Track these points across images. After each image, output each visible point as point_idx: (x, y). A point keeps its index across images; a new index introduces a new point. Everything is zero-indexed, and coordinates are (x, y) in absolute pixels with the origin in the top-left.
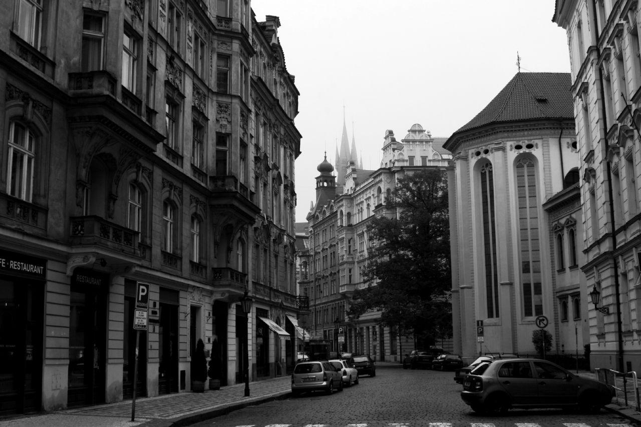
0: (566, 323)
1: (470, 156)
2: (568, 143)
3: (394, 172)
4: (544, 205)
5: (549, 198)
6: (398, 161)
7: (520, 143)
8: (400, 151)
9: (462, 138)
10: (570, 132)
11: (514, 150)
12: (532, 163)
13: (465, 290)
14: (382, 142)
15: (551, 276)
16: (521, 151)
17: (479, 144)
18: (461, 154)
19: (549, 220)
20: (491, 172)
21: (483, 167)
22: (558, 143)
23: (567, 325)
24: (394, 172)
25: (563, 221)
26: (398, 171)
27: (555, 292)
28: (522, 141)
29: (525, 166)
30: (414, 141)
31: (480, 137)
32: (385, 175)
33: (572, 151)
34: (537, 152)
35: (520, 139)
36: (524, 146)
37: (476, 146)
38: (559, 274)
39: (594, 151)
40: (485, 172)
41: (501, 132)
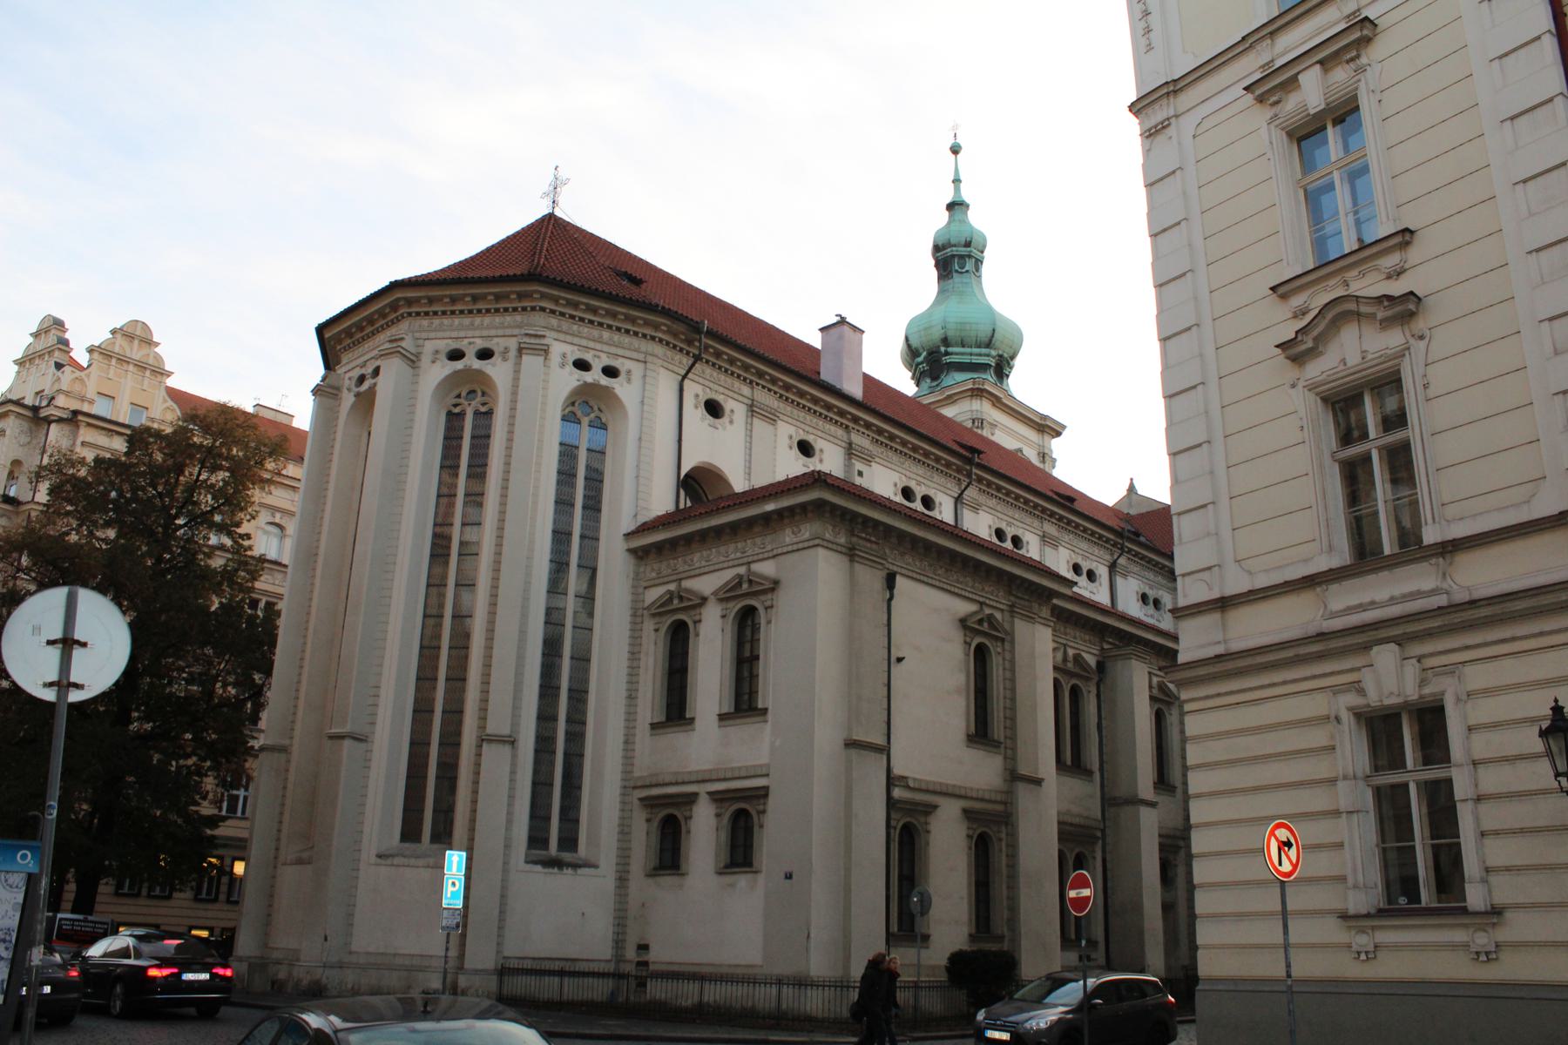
0: (668, 880)
1: (425, 360)
3: (48, 421)
4: (628, 536)
6: (67, 394)
7: (588, 357)
9: (410, 302)
11: (570, 367)
13: (347, 743)
14: (21, 342)
16: (588, 377)
18: (403, 344)
22: (676, 387)
24: (48, 421)
25: (707, 584)
26: (60, 420)
29: (585, 421)
30: (123, 360)
31: (470, 312)
32: (18, 422)
33: (703, 419)
35: (591, 344)
36: (597, 367)
39: (1412, 232)
41: (543, 309)
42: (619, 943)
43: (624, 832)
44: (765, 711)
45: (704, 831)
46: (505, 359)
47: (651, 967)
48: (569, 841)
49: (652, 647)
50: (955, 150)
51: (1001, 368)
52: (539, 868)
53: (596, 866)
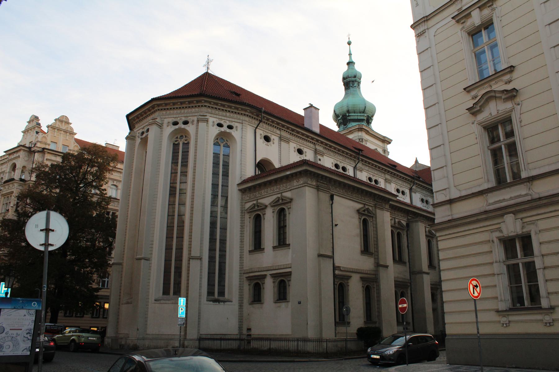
0: (257, 306)
1: (165, 125)
3: (34, 152)
4: (238, 185)
5: (243, 179)
6: (41, 142)
7: (222, 122)
8: (44, 135)
9: (159, 105)
11: (216, 126)
13: (143, 261)
14: (24, 125)
15: (239, 257)
16: (222, 129)
17: (179, 114)
19: (242, 199)
23: (262, 308)
24: (34, 152)
27: (242, 272)
29: (222, 145)
30: (59, 130)
32: (24, 153)
35: (223, 118)
36: (225, 126)
37: (175, 116)
39: (514, 67)
40: (179, 144)
41: (205, 106)
42: (240, 328)
44: (289, 245)
45: (269, 288)
46: (193, 124)
47: (252, 336)
48: (222, 293)
49: (248, 223)
50: (349, 43)
51: (369, 120)
52: (211, 303)
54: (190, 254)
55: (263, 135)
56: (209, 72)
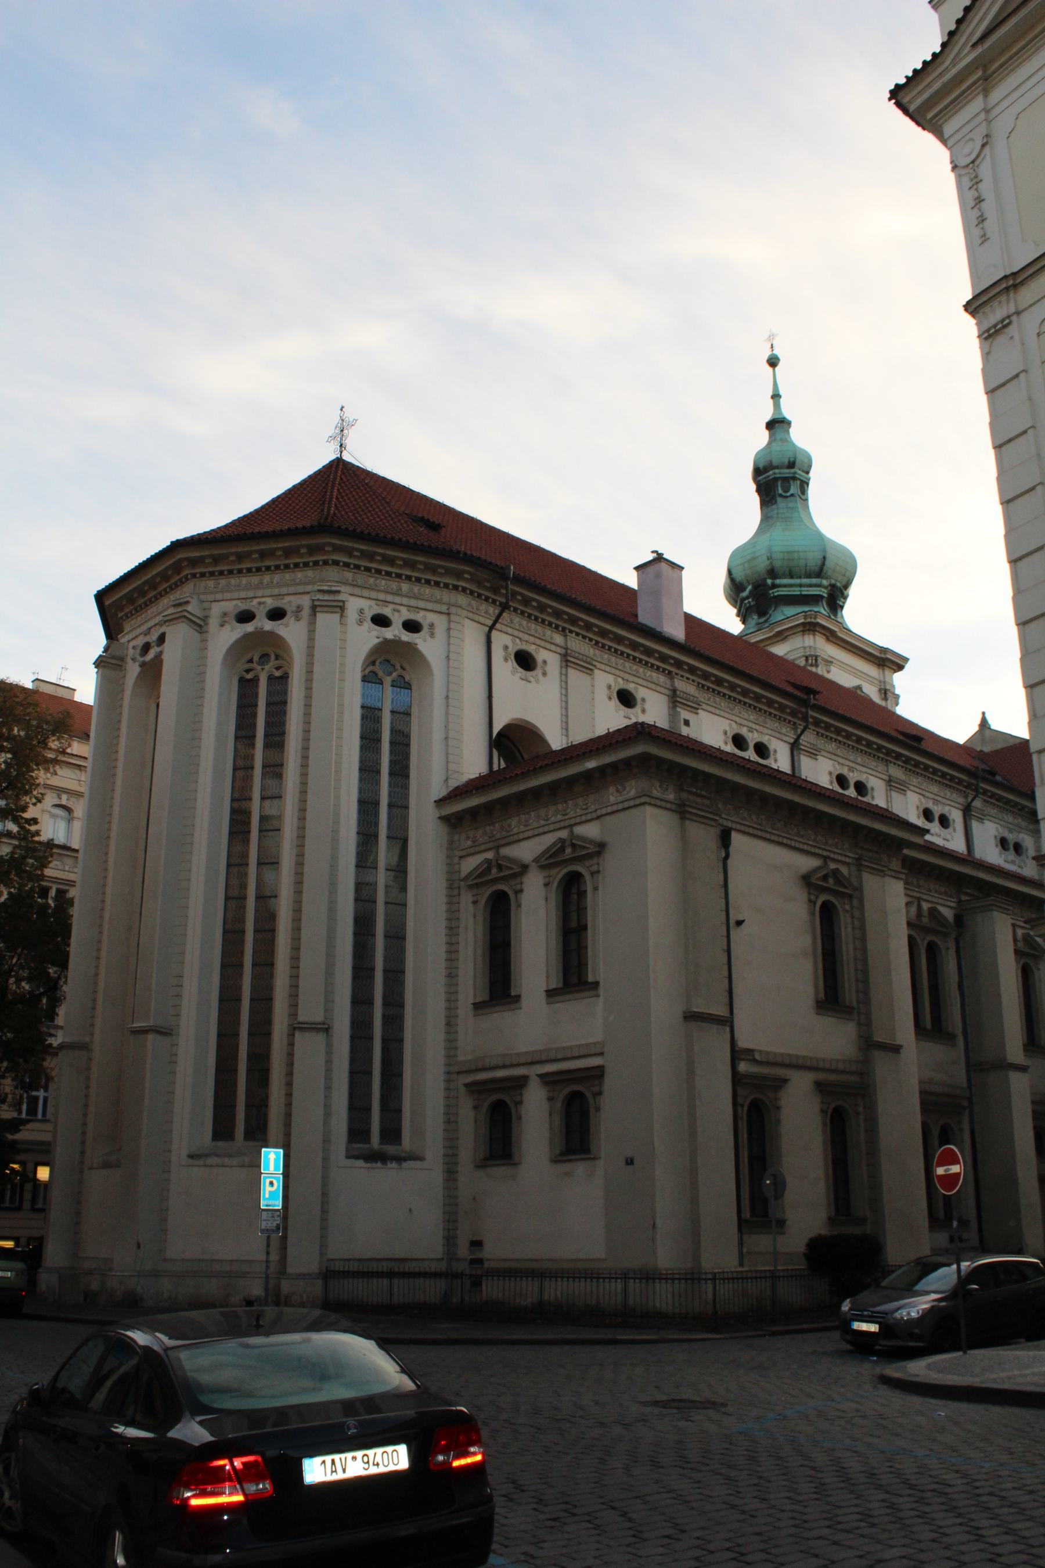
1: (213, 623)
2: (506, 647)
4: (440, 802)
7: (387, 611)
9: (193, 562)
10: (512, 621)
11: (368, 624)
12: (407, 678)
13: (150, 1037)
16: (389, 633)
18: (189, 608)
19: (451, 846)
20: (280, 682)
21: (251, 661)
22: (482, 639)
25: (526, 851)
27: (453, 1071)
28: (391, 606)
29: (387, 681)
34: (428, 646)
35: (389, 598)
36: (397, 621)
38: (475, 1016)
41: (336, 563)
42: (450, 1240)
43: (451, 1120)
44: (596, 985)
47: (486, 1265)
48: (392, 1133)
50: (773, 362)
51: (836, 598)
52: (360, 1163)
53: (421, 1158)
54: (294, 1014)
55: (512, 650)
56: (346, 457)
